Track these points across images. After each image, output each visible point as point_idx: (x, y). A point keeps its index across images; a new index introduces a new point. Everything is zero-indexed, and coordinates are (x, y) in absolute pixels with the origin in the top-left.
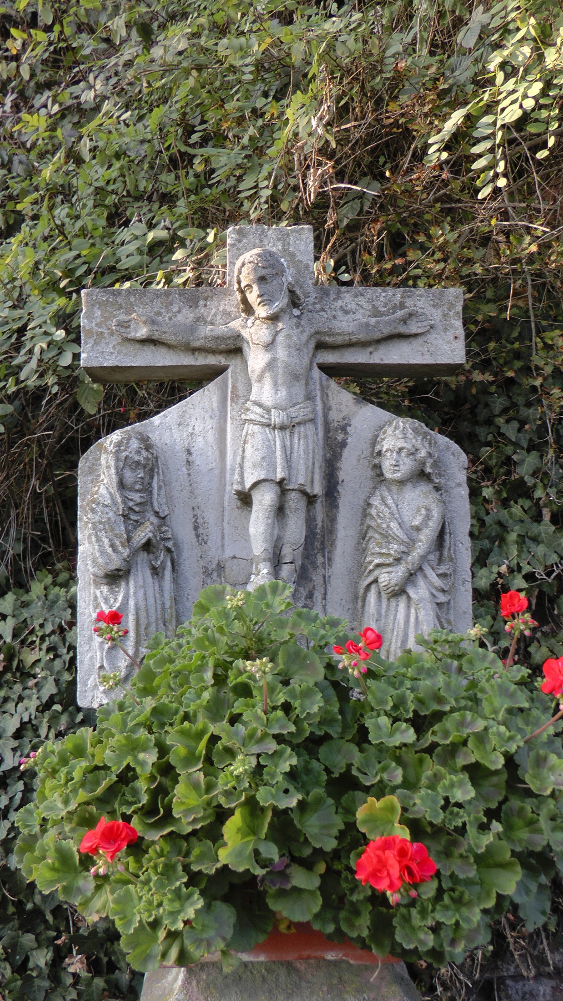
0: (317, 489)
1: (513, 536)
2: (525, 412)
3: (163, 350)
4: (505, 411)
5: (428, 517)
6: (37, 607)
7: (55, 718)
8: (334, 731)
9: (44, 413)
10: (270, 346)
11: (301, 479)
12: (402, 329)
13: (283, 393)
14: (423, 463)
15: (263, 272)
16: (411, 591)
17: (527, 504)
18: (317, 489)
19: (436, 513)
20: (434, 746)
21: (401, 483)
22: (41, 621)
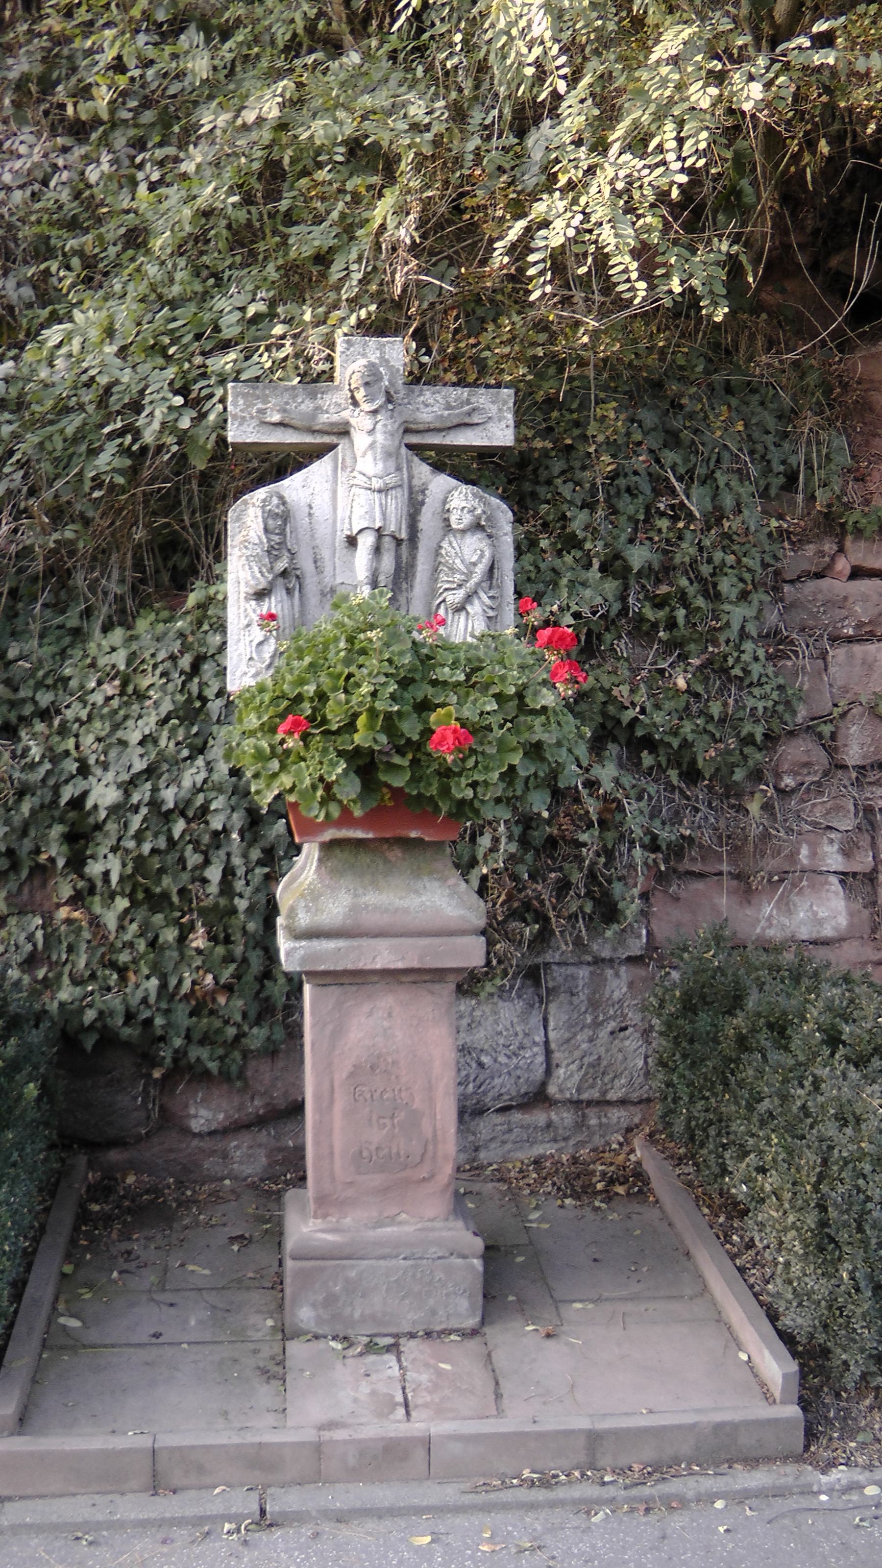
0: (404, 535)
1: (564, 581)
2: (580, 475)
3: (291, 431)
4: (563, 473)
5: (482, 556)
6: (146, 639)
7: (173, 731)
8: (418, 676)
9: (150, 467)
10: (371, 432)
11: (393, 528)
12: (467, 420)
13: (380, 465)
14: (479, 518)
15: (368, 379)
16: (469, 608)
17: (579, 554)
18: (404, 535)
19: (487, 554)
20: (476, 683)
21: (463, 532)
22: (152, 651)
